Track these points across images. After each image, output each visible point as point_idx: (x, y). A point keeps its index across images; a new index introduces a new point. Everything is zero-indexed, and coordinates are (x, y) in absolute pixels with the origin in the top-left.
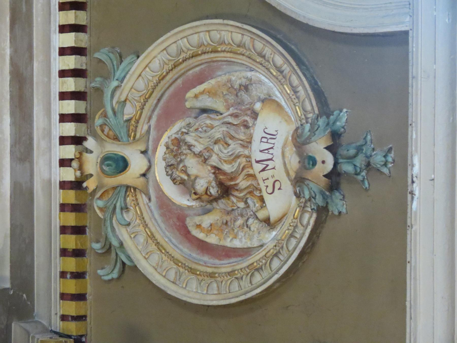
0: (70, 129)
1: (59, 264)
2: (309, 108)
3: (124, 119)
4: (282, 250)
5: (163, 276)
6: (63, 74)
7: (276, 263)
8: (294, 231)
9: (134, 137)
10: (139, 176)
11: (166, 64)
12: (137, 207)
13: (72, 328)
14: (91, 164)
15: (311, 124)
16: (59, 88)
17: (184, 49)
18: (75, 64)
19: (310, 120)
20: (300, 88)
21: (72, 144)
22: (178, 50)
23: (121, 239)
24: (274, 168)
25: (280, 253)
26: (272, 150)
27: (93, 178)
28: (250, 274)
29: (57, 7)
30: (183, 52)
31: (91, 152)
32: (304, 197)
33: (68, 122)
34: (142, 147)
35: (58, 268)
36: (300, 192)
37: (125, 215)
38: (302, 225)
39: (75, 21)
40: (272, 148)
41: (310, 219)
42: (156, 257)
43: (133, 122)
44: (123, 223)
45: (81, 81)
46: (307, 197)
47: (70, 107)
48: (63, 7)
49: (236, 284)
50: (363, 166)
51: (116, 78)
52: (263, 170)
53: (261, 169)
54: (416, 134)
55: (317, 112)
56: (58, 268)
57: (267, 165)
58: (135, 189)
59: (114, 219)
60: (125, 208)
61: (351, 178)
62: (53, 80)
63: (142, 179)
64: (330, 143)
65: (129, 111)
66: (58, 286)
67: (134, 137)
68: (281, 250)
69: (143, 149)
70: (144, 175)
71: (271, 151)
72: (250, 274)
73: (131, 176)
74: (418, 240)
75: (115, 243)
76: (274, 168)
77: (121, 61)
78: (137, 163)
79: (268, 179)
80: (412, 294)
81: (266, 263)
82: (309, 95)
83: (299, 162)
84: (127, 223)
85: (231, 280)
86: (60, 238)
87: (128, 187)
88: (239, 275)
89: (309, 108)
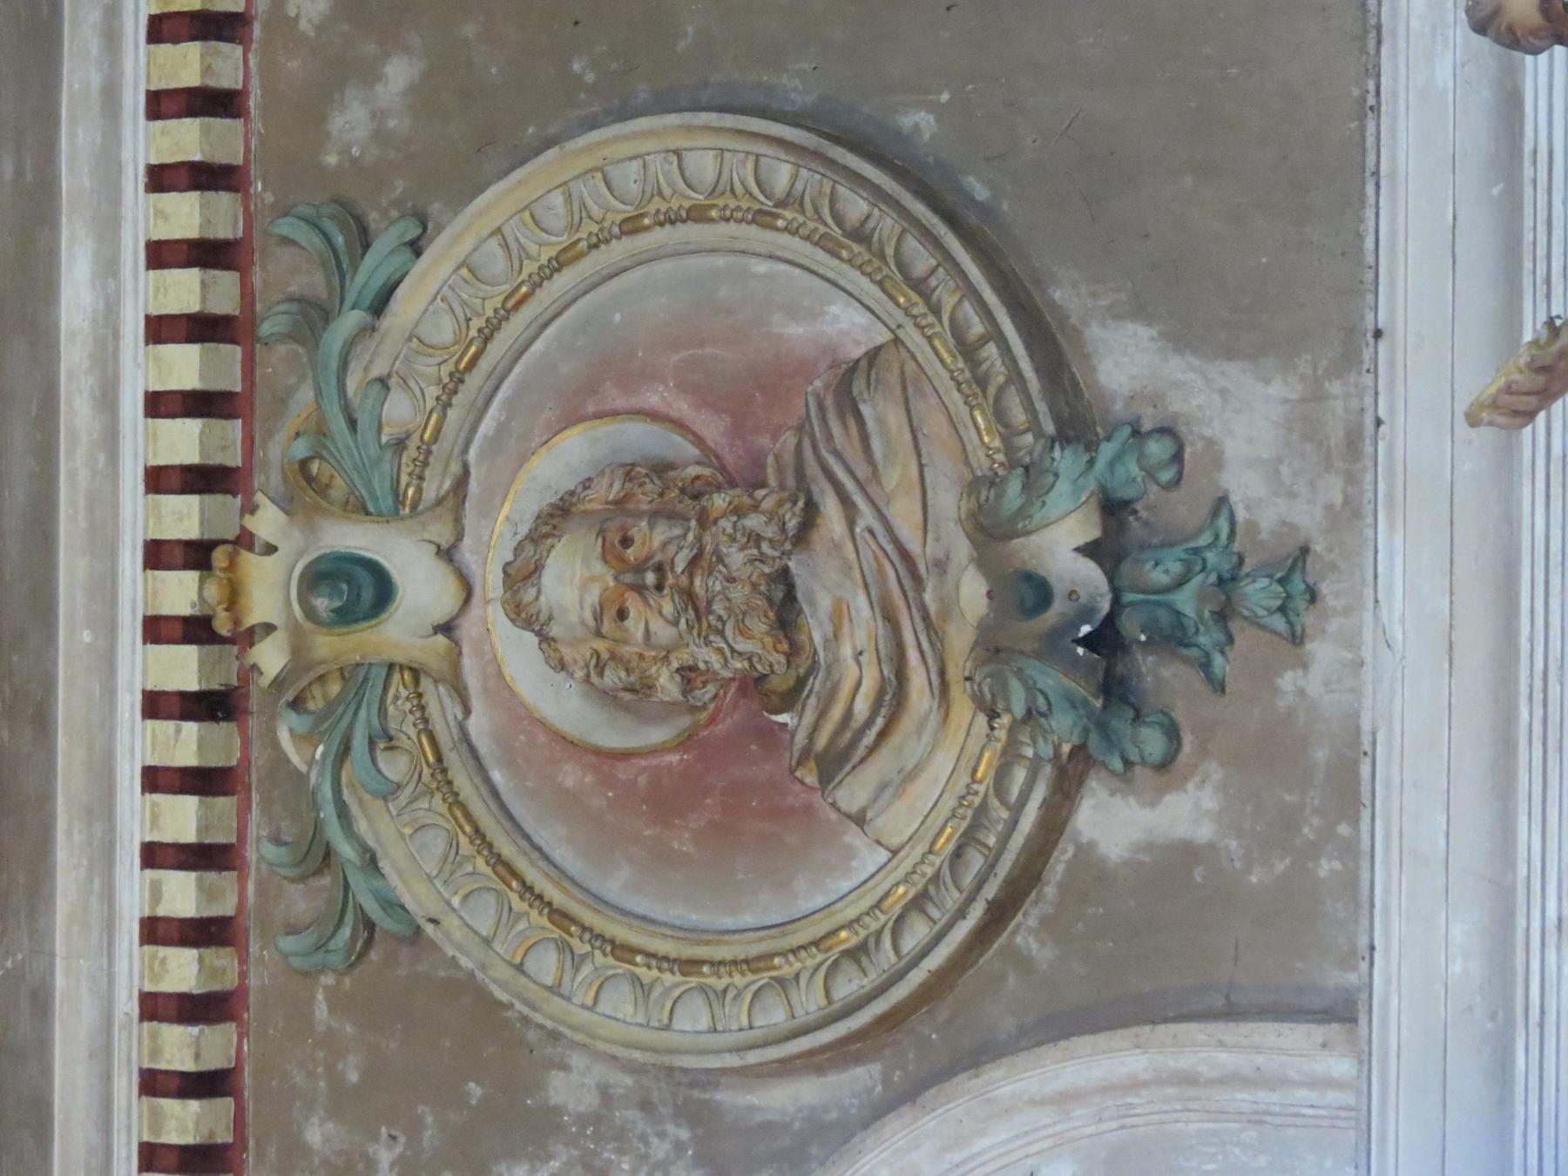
0: (184, 517)
1: (136, 968)
2: (1019, 417)
4: (938, 888)
5: (513, 966)
6: (158, 480)
7: (917, 933)
9: (414, 506)
10: (431, 631)
11: (529, 257)
13: (184, 1122)
14: (268, 590)
16: (146, 528)
18: (200, 682)
20: (991, 350)
21: (193, 38)
25: (931, 899)
28: (824, 969)
29: (142, 179)
31: (270, 549)
32: (1008, 710)
33: (173, 416)
34: (441, 531)
35: (138, 754)
36: (993, 695)
37: (381, 758)
39: (204, 299)
43: (411, 452)
46: (1019, 710)
47: (184, 215)
48: (161, 29)
51: (351, 296)
55: (1050, 428)
56: (138, 754)
58: (416, 673)
60: (382, 739)
62: (127, 131)
63: (441, 639)
64: (1094, 533)
65: (399, 410)
66: (136, 968)
67: (414, 506)
68: (932, 889)
70: (446, 628)
72: (824, 969)
73: (401, 632)
74: (1391, 1137)
77: (366, 246)
78: (422, 588)
80: (1402, 269)
81: (879, 933)
82: (1020, 374)
83: (990, 594)
85: (755, 987)
86: (147, 282)
88: (786, 971)
89: (1019, 417)
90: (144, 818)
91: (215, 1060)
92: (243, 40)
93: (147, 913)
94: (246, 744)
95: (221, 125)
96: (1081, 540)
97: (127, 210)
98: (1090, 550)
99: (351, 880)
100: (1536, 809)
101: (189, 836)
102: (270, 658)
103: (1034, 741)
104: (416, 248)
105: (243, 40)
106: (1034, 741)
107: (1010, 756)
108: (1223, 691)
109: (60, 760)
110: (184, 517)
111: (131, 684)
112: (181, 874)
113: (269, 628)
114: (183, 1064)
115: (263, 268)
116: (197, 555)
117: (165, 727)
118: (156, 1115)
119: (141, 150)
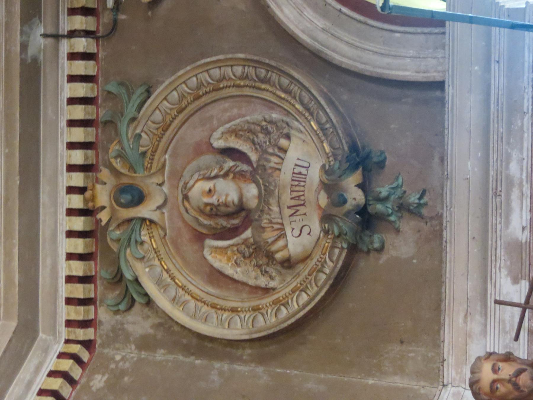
3: (140, 152)
8: (323, 266)
12: (152, 240)
14: (103, 196)
15: (340, 161)
17: (204, 82)
19: (339, 157)
22: (198, 83)
23: (137, 274)
24: (305, 214)
26: (303, 207)
27: (105, 210)
29: (65, 190)
30: (203, 85)
38: (331, 260)
40: (303, 195)
41: (340, 254)
44: (137, 256)
45: (91, 108)
48: (73, 11)
49: (260, 318)
50: (395, 207)
52: (292, 215)
53: (290, 214)
54: (451, 247)
57: (298, 211)
59: (128, 251)
61: (382, 217)
69: (160, 182)
71: (302, 198)
75: (128, 275)
76: (305, 214)
79: (295, 221)
84: (141, 256)
87: (144, 220)
90: (65, 268)
91: (91, 139)
92: (95, 260)
93: (67, 338)
94: (97, 156)
95: (90, 108)
96: (355, 184)
97: (59, 311)
98: (359, 186)
99: (128, 286)
100: (493, 314)
101: (81, 274)
102: (104, 216)
103: (341, 243)
105: (95, 260)
106: (341, 243)
107: (333, 247)
108: (399, 231)
109: (40, 287)
111: (62, 295)
112: (78, 174)
113: (104, 208)
114: (78, 369)
115: (99, 329)
116: (81, 190)
117: (72, 308)
118: (69, 266)
119: (66, 4)
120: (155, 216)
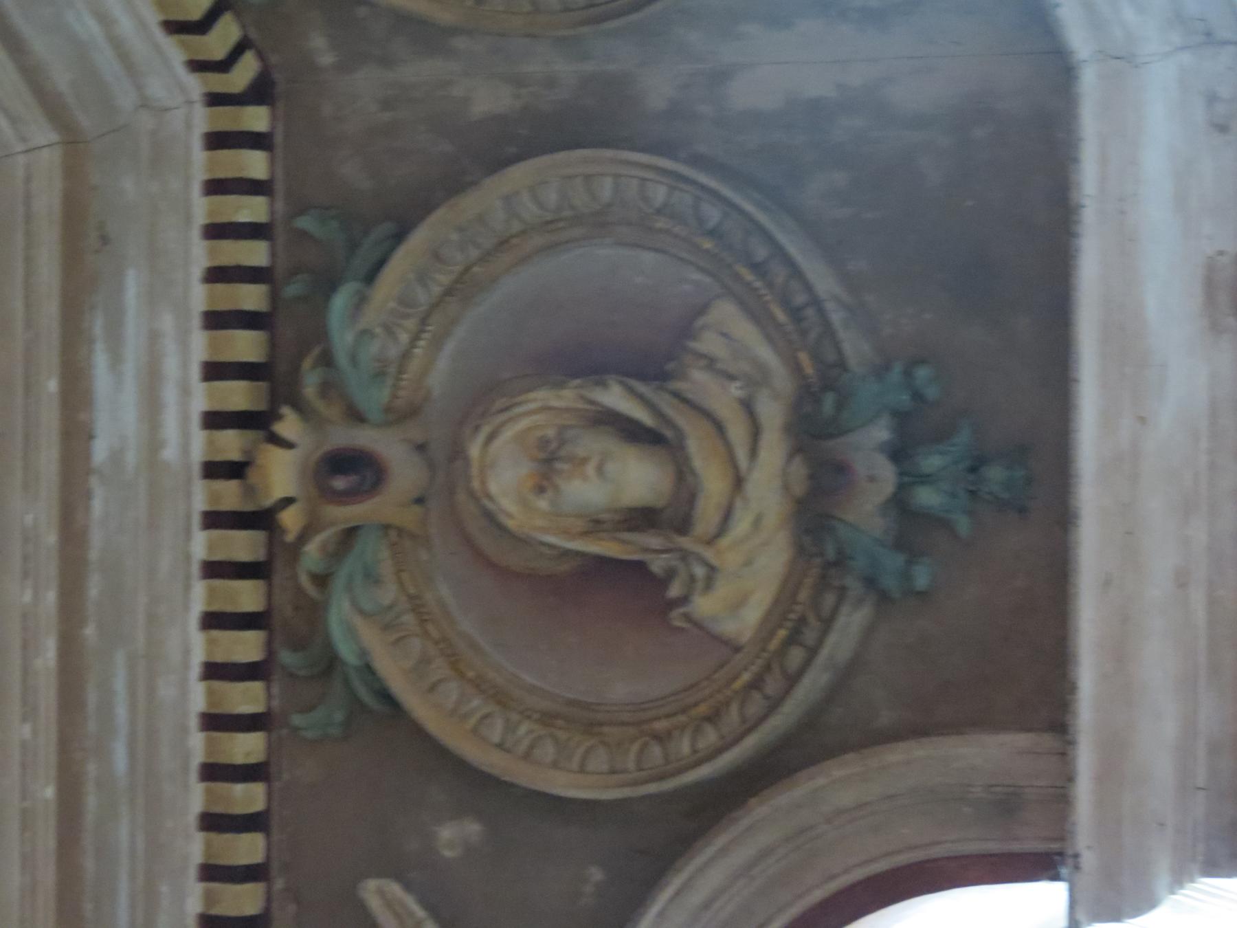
0: (231, 444)
42: (452, 691)
104: (399, 237)
110: (231, 444)
113: (288, 501)
116: (234, 470)
120: (409, 518)
